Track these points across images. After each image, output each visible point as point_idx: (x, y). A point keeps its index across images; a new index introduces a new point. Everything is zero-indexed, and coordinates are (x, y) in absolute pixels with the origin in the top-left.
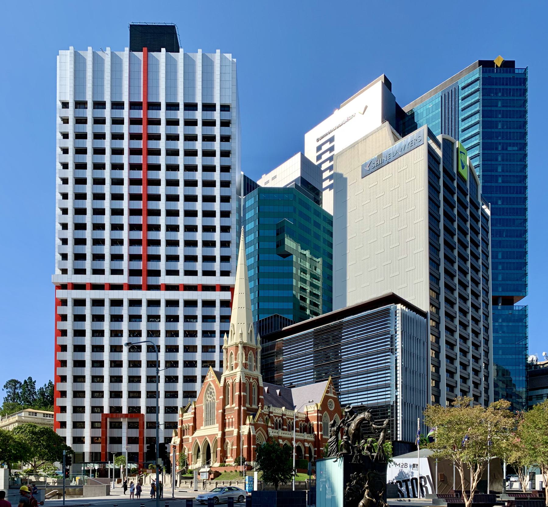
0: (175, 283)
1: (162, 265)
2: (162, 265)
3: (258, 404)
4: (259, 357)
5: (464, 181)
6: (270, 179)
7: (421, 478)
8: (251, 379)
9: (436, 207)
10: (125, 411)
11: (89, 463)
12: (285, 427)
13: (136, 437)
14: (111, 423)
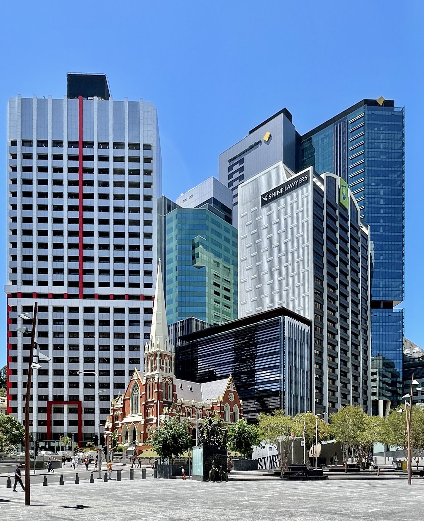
0: (107, 296)
1: (96, 278)
2: (96, 278)
3: (172, 399)
4: (173, 362)
5: (346, 210)
7: (273, 456)
8: (167, 379)
9: (320, 233)
10: (66, 399)
12: (194, 415)
13: (85, 274)
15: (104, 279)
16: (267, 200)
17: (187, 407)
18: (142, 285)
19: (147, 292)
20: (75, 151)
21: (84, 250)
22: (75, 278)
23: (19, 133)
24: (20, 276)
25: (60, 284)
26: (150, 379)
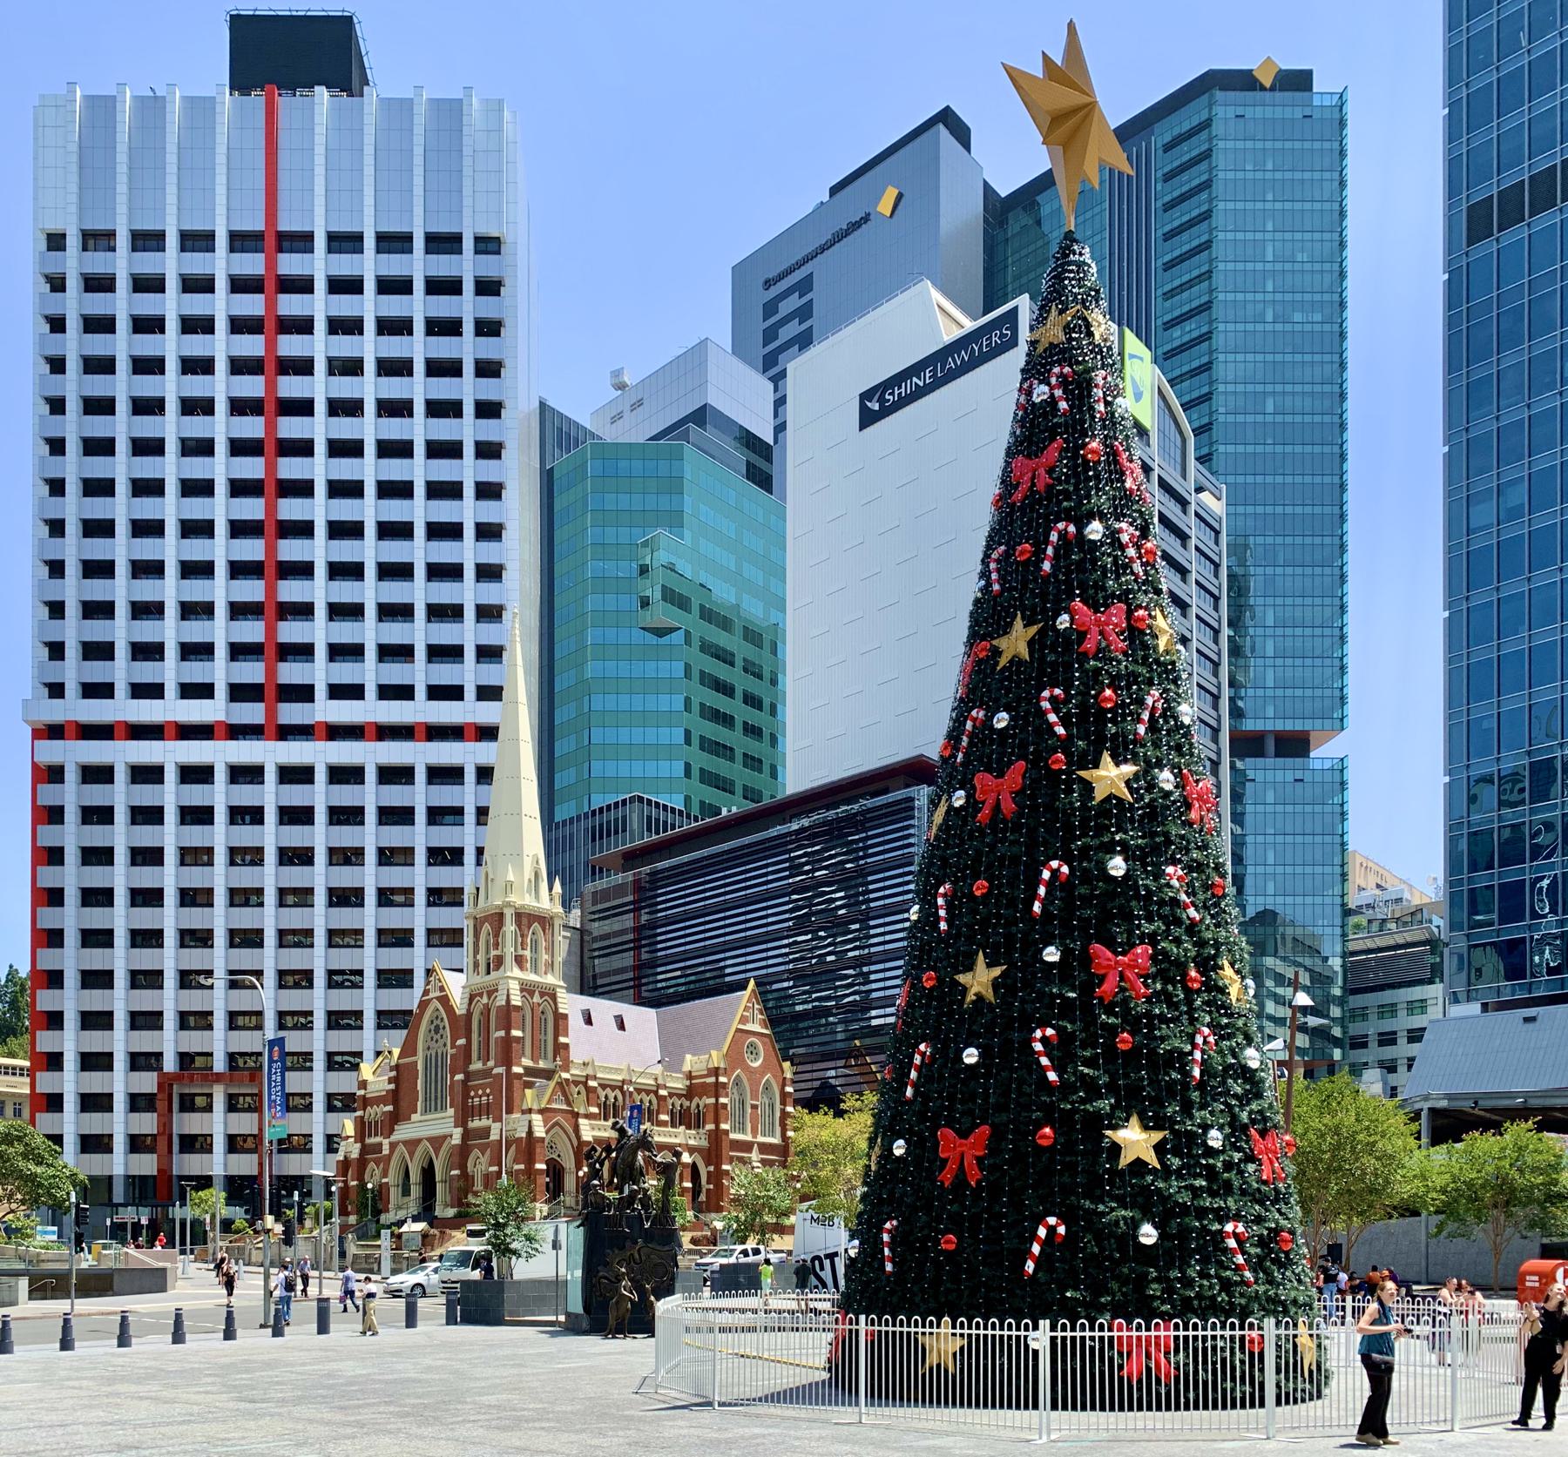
2: (320, 672)
6: (626, 414)
10: (219, 1065)
11: (125, 1205)
14: (182, 1096)
15: (346, 673)
16: (878, 404)
17: (604, 1087)
18: (470, 693)
19: (485, 713)
20: (252, 264)
21: (280, 582)
22: (252, 672)
23: (73, 209)
24: (73, 671)
25: (203, 691)
26: (481, 995)
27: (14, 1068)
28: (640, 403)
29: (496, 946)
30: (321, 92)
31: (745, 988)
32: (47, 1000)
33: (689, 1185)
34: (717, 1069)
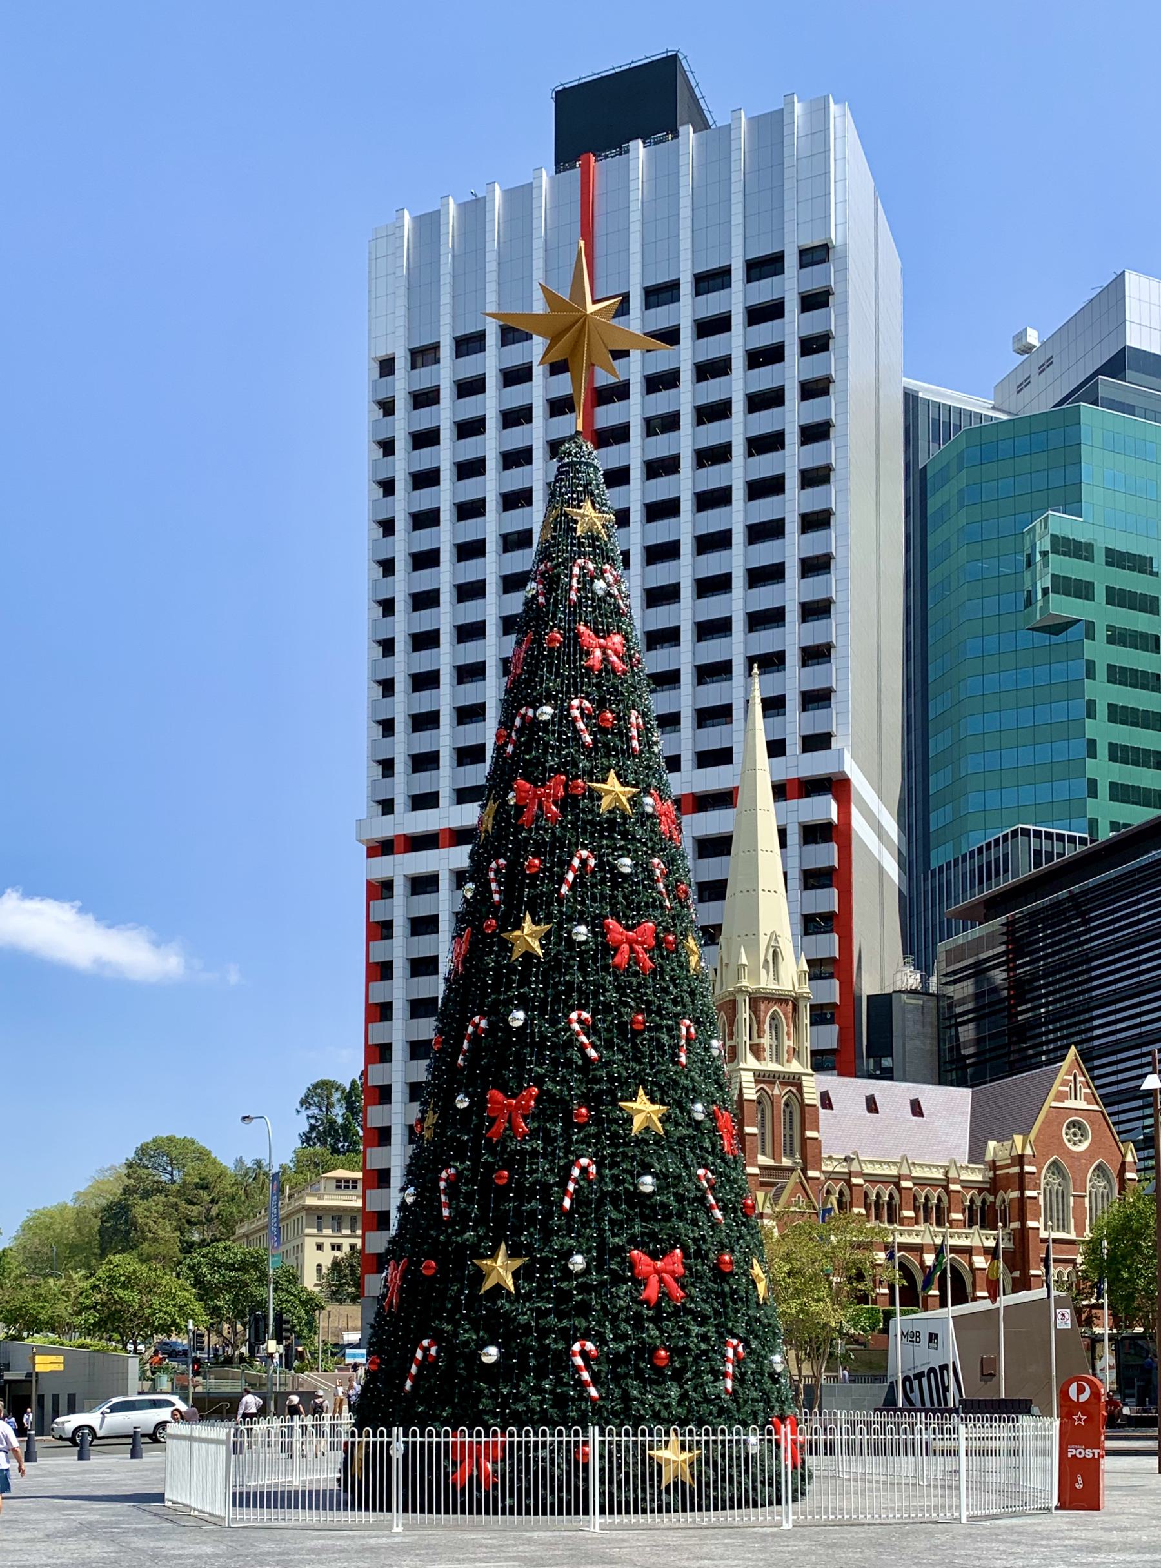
24: (401, 785)
27: (347, 1181)
28: (1050, 362)
29: (731, 1035)
30: (638, 148)
31: (1062, 1058)
32: (376, 1116)
33: (937, 1293)
34: (1021, 1157)
